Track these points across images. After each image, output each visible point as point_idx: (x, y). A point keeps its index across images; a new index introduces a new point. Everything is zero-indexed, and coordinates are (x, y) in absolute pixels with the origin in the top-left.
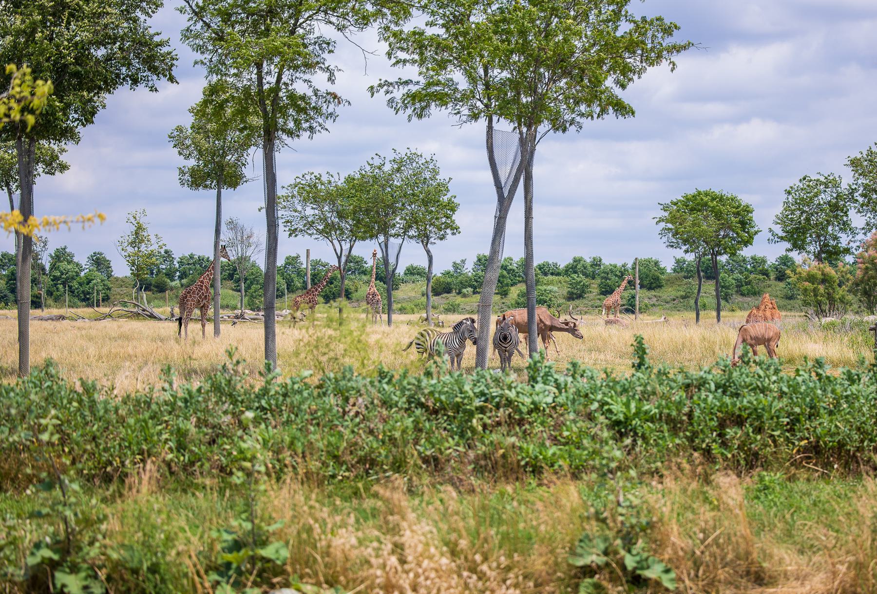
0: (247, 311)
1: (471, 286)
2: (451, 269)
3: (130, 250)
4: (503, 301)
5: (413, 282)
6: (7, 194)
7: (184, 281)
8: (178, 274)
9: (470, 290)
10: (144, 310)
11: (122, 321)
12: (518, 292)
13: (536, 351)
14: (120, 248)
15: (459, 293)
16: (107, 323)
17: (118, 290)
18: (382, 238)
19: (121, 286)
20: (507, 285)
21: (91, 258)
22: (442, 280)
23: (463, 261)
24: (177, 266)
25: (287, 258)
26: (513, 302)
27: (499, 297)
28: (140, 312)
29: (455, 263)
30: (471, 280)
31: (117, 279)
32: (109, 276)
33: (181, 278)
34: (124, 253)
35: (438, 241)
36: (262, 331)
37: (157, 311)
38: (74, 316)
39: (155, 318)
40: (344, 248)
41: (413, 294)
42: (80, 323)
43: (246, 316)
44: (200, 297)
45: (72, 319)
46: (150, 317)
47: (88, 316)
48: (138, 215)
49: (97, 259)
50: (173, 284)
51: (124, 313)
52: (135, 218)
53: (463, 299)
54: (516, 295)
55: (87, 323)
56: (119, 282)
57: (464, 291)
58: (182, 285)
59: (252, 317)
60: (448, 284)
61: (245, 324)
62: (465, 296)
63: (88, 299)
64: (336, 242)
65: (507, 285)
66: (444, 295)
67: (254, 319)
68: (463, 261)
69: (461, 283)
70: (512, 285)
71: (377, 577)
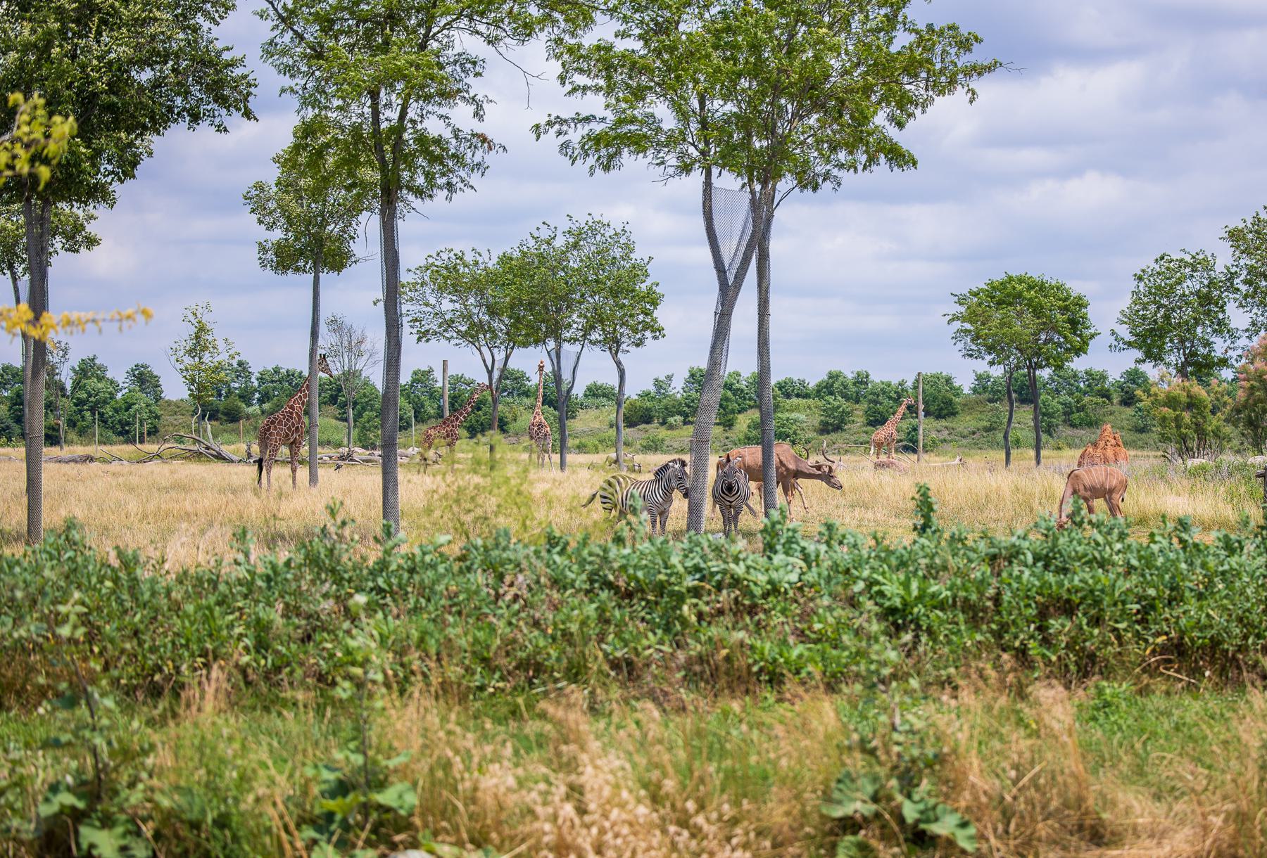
0: (356, 449)
1: (680, 413)
2: (652, 389)
3: (188, 360)
4: (727, 435)
5: (597, 407)
6: (10, 280)
7: (266, 406)
8: (257, 395)
9: (679, 418)
10: (208, 448)
11: (177, 463)
12: (748, 422)
13: (774, 507)
14: (174, 358)
15: (664, 423)
16: (154, 466)
17: (171, 419)
18: (551, 344)
19: (175, 413)
20: (733, 412)
21: (132, 373)
22: (638, 404)
23: (669, 378)
24: (256, 384)
25: (415, 373)
26: (742, 436)
27: (721, 428)
28: (203, 450)
29: (657, 380)
30: (680, 404)
31: (169, 403)
32: (158, 399)
33: (261, 401)
34: (179, 366)
35: (633, 349)
36: (379, 479)
37: (226, 450)
38: (106, 456)
39: (224, 459)
40: (497, 358)
41: (596, 425)
42: (115, 466)
43: (355, 457)
44: (289, 429)
45: (104, 461)
46: (216, 457)
47: (127, 456)
48: (200, 310)
49: (141, 374)
50: (250, 410)
51: (179, 452)
52: (194, 314)
53: (669, 432)
54: (745, 426)
55: (126, 467)
56: (173, 407)
57: (671, 420)
58: (263, 412)
59: (364, 457)
60: (648, 410)
61: (354, 468)
62: (671, 427)
63: (128, 432)
64: (485, 350)
65: (733, 412)
66: (642, 426)
67: (367, 461)
68: (669, 378)
69: (666, 409)
70: (740, 412)
71: (545, 833)
